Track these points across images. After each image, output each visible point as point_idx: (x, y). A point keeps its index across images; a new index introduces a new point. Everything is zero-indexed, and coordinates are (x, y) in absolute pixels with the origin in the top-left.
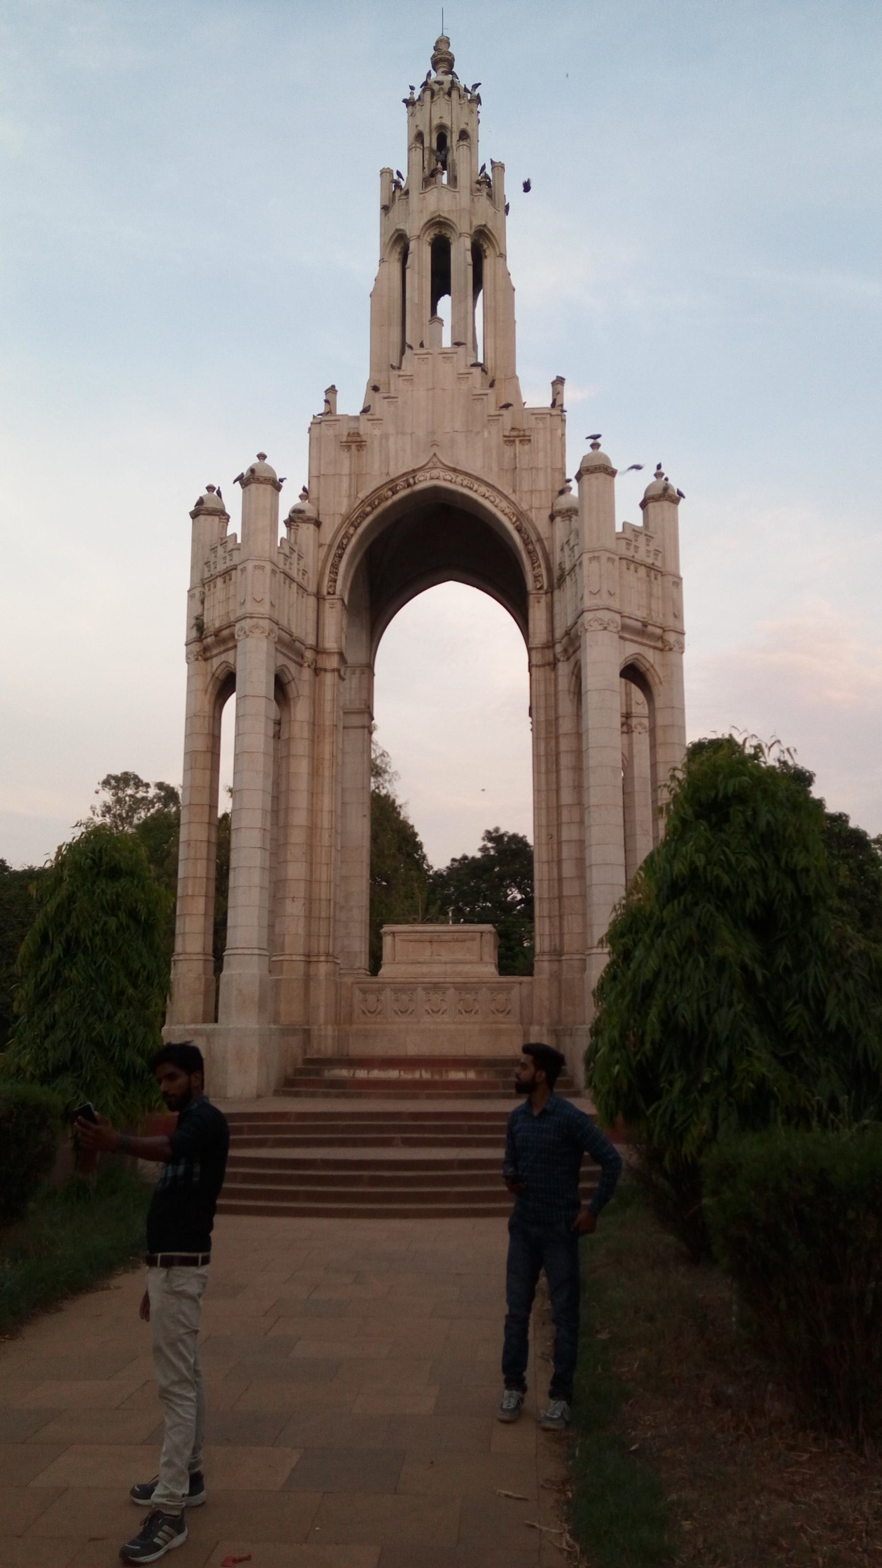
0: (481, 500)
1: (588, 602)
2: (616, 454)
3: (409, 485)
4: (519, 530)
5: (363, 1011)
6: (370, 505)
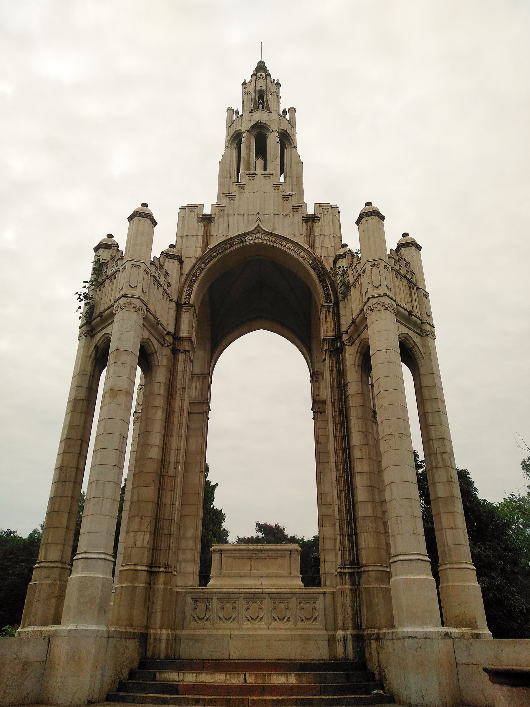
3: (242, 242)
4: (314, 269)
5: (194, 618)
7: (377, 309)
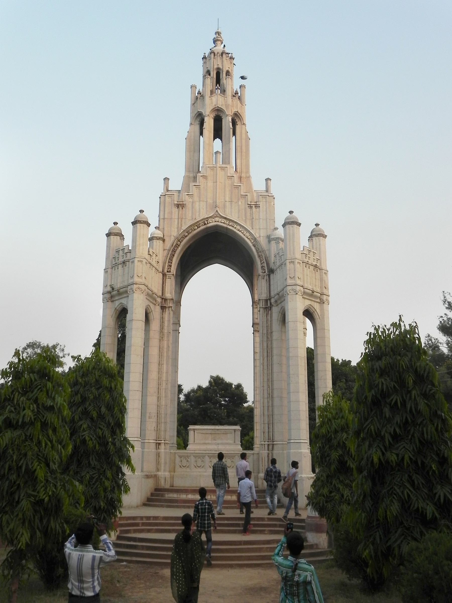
0: (238, 232)
1: (289, 282)
2: (299, 216)
3: (205, 224)
4: (254, 246)
6: (187, 232)
7: (291, 294)
